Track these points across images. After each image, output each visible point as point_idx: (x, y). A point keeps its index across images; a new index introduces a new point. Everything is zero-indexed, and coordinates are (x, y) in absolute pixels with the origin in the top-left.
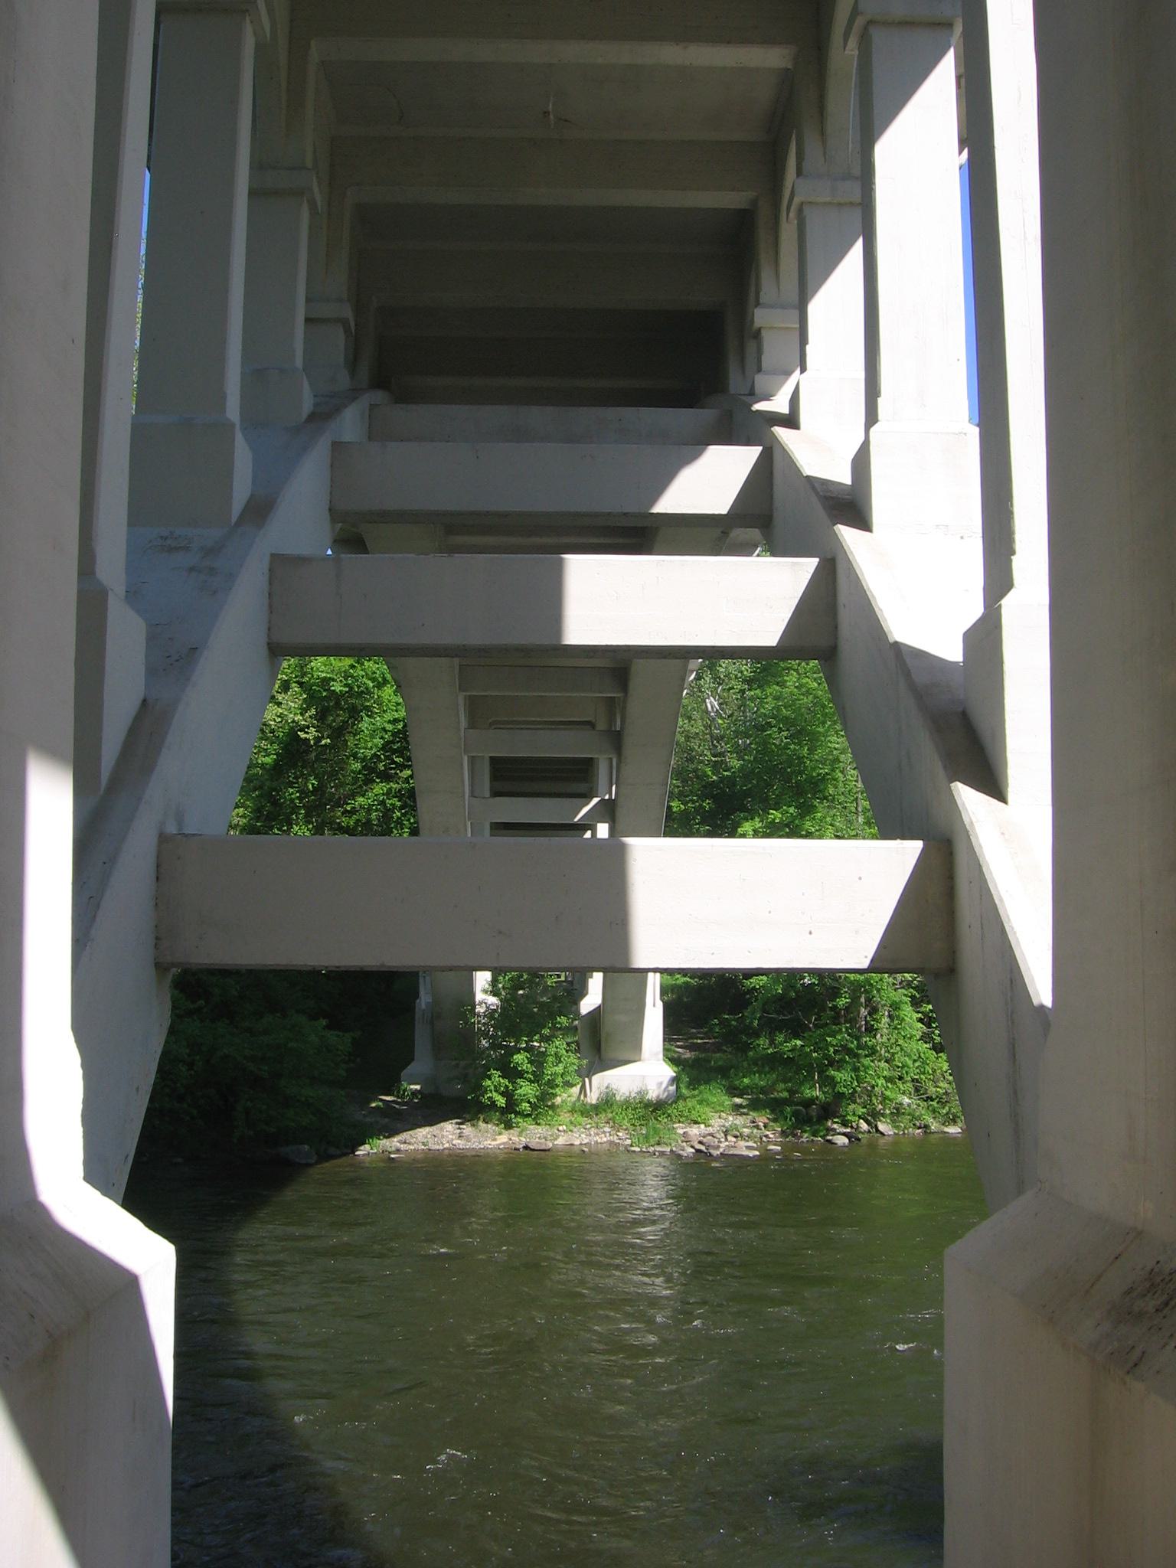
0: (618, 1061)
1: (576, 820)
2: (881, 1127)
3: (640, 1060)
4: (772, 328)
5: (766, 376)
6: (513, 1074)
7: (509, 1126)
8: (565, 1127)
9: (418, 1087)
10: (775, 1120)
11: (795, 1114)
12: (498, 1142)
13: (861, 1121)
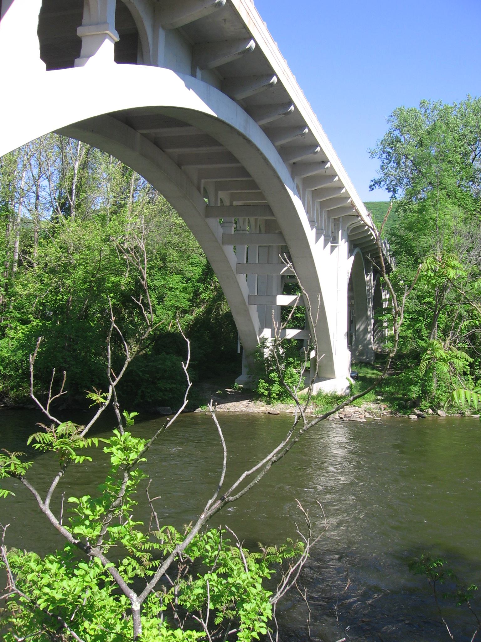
0: (326, 378)
1: (281, 273)
2: (439, 412)
3: (335, 378)
4: (86, 36)
5: (82, 59)
6: (271, 382)
7: (269, 403)
8: (293, 405)
9: (242, 386)
10: (389, 407)
11: (399, 405)
12: (260, 410)
13: (430, 409)
